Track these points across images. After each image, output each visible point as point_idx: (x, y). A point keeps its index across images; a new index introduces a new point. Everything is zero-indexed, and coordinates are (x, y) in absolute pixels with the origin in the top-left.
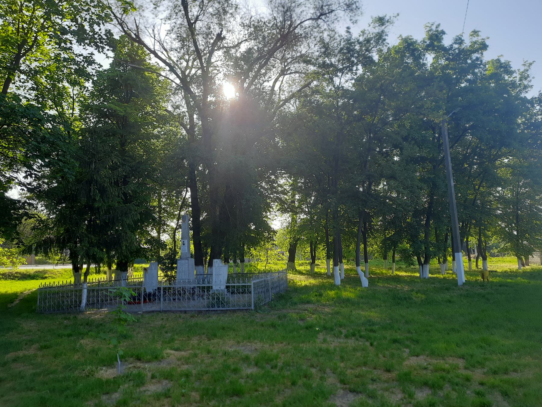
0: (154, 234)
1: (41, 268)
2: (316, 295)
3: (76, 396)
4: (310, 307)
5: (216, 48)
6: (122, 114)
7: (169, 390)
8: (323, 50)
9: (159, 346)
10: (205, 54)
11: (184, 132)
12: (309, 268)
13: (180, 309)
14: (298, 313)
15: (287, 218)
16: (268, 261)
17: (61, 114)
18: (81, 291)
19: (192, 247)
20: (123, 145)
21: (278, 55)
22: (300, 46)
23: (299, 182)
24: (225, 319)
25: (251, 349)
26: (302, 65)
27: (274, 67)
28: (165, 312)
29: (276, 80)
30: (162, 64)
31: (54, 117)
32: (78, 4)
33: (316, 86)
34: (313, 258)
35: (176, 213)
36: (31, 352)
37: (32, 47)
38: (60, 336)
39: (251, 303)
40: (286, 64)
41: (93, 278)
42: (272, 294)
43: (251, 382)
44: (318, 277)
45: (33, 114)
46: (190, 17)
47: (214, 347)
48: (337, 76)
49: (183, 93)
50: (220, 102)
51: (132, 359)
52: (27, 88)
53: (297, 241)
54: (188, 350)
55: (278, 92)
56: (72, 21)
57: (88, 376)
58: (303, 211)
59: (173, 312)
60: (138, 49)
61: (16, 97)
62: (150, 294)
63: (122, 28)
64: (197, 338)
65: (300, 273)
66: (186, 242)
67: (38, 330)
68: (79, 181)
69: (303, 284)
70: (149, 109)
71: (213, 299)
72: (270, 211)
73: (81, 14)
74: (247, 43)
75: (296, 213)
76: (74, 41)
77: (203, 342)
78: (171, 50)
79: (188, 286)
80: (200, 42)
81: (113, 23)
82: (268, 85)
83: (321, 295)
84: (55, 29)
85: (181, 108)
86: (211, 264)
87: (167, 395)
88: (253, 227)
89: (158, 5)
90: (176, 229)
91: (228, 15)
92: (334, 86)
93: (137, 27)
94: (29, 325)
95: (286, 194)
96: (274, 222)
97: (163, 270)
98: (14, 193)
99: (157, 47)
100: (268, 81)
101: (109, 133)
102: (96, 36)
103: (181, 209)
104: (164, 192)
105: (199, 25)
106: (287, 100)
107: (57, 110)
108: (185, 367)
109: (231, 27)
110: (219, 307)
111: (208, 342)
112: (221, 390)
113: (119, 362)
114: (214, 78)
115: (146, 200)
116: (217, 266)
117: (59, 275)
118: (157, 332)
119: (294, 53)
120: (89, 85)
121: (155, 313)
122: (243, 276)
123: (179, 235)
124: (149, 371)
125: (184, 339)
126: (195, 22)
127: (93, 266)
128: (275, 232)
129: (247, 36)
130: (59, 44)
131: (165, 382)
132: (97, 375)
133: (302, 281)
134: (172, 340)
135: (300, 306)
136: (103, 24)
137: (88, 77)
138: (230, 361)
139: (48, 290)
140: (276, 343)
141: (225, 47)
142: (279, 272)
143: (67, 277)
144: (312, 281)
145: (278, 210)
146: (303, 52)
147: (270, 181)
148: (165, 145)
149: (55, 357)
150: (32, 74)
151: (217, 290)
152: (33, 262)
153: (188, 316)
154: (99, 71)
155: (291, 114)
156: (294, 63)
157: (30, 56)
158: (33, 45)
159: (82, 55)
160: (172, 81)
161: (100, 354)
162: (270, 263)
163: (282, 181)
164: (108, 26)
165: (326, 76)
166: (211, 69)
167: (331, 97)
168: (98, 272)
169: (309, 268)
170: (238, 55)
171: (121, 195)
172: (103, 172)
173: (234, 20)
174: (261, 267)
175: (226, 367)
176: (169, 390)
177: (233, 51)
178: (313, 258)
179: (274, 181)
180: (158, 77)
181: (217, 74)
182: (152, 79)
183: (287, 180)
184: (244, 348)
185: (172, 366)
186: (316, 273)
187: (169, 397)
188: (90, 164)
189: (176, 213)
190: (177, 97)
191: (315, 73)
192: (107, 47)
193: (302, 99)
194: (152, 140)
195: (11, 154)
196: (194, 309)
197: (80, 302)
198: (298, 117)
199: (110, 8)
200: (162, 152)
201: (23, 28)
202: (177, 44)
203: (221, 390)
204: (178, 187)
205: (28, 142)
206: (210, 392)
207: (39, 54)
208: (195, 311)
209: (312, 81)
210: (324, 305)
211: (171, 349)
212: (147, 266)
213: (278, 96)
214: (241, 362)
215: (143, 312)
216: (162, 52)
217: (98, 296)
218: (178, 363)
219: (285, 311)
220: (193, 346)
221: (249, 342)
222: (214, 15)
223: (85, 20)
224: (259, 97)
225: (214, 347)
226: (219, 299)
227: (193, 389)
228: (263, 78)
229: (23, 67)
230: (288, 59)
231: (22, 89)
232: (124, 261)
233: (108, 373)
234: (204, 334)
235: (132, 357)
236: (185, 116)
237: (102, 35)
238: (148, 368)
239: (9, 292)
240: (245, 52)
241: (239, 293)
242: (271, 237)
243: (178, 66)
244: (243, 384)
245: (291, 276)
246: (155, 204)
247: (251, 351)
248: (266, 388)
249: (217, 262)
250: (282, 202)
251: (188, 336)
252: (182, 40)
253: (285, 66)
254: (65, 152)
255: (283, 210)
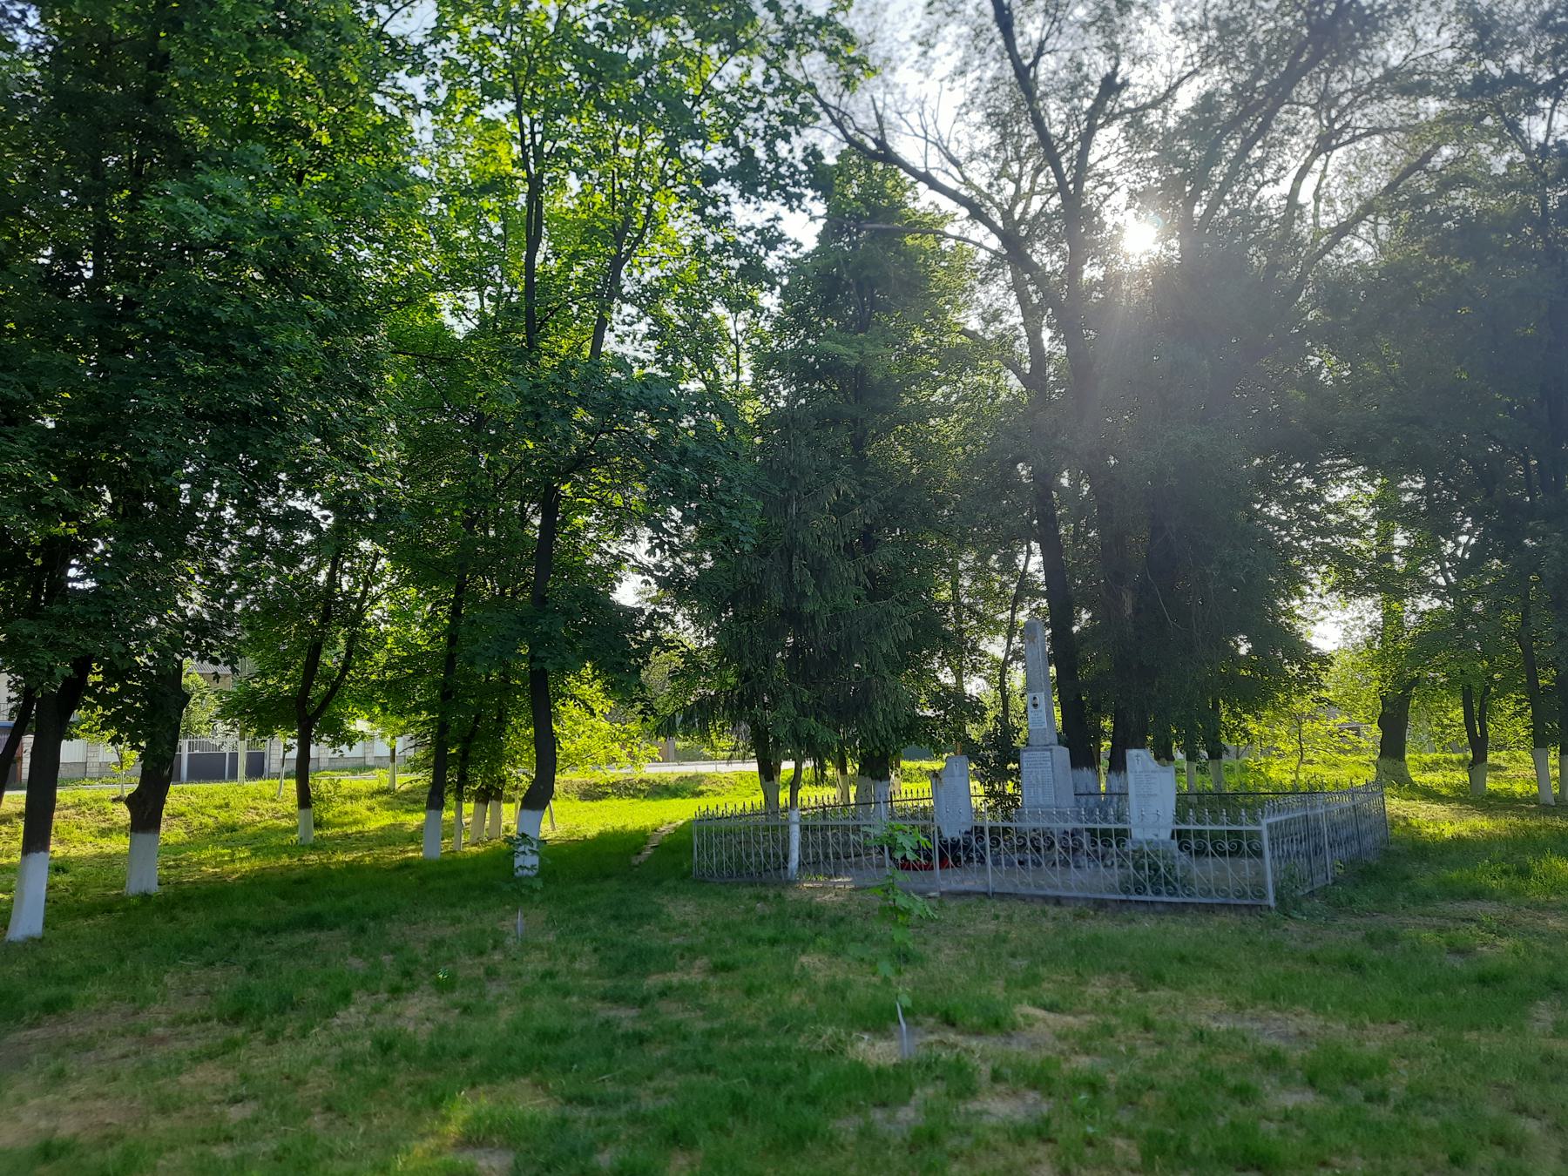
0: (947, 678)
1: (689, 769)
2: (1505, 872)
3: (811, 1100)
4: (1485, 910)
5: (1100, 122)
6: (853, 363)
7: (1047, 1121)
8: (1471, 36)
9: (997, 991)
10: (1070, 146)
11: (1014, 383)
12: (1461, 777)
13: (1041, 893)
14: (1440, 930)
15: (1366, 611)
16: (1310, 755)
17: (713, 388)
18: (786, 827)
19: (1058, 715)
20: (858, 444)
21: (1306, 90)
22: (1382, 42)
23: (1406, 491)
24: (1181, 933)
25: (1290, 1028)
26: (1394, 103)
27: (1293, 132)
28: (1002, 896)
29: (1304, 171)
30: (947, 205)
31: (698, 396)
32: (735, 99)
33: (1456, 160)
34: (1479, 746)
35: (1001, 616)
36: (694, 975)
37: (642, 233)
38: (753, 941)
39: (1264, 885)
40: (1334, 113)
41: (810, 795)
42: (1332, 862)
43: (1300, 1133)
44: (1505, 809)
45: (655, 398)
46: (1020, 51)
47: (1160, 1013)
48: (1534, 111)
49: (1009, 275)
50: (1119, 277)
51: (931, 1021)
52: (639, 336)
53: (1407, 688)
54: (1083, 1013)
55: (1311, 207)
56: (725, 145)
57: (830, 1053)
58: (1426, 586)
59: (1022, 898)
60: (883, 177)
61: (621, 363)
62: (955, 845)
63: (843, 131)
64: (1105, 979)
65: (1429, 794)
66: (1041, 698)
67: (704, 924)
68: (762, 551)
69: (1449, 831)
70: (918, 337)
71: (1138, 867)
72: (1302, 595)
73: (745, 122)
74: (1198, 80)
75: (1400, 595)
76: (734, 193)
77: (1124, 992)
78: (972, 157)
79: (1058, 826)
80: (1053, 115)
81: (819, 124)
82: (1273, 195)
83: (1524, 872)
84: (689, 176)
85: (1005, 317)
86: (1118, 764)
87: (1042, 1133)
88: (1243, 651)
89: (932, 41)
90: (1006, 663)
91: (1135, 13)
92: (1525, 149)
93: (879, 118)
94: (682, 909)
95: (1357, 534)
96: (1319, 628)
97: (981, 778)
98: (629, 592)
99: (935, 160)
100: (1276, 182)
101: (828, 419)
102: (783, 170)
103: (1015, 603)
104: (969, 557)
105: (1048, 64)
106: (1344, 229)
107: (703, 380)
108: (1083, 1062)
109: (1145, 45)
110: (1158, 893)
111: (1140, 996)
112: (1204, 1145)
113: (903, 1025)
114: (1097, 213)
115: (925, 586)
116: (1139, 768)
117: (728, 787)
118: (986, 951)
119: (1360, 73)
120: (770, 301)
121: (973, 899)
122: (1221, 801)
123: (1017, 678)
124: (984, 1059)
125: (1067, 979)
126: (1035, 63)
127: (808, 764)
128: (1325, 660)
129: (1196, 59)
130: (699, 211)
131: (1032, 1096)
132: (851, 1053)
133: (1442, 823)
134: (1031, 980)
135: (1447, 907)
136: (798, 133)
137: (770, 278)
138: (1222, 1061)
139: (704, 825)
140: (1372, 1021)
141: (1129, 111)
142: (1353, 791)
143: (748, 792)
144: (1482, 824)
145: (1332, 589)
146: (1395, 62)
147: (1296, 498)
148: (965, 429)
149: (749, 992)
150: (649, 298)
151: (1149, 843)
152: (672, 754)
153: (1066, 912)
154: (793, 262)
155: (1361, 267)
156: (1363, 105)
157: (641, 256)
158: (645, 227)
159: (752, 228)
160: (980, 245)
161: (851, 995)
162: (1311, 762)
163: (1339, 493)
164: (811, 136)
165: (1488, 121)
166: (1088, 184)
167: (1513, 186)
168: (820, 780)
169: (1461, 777)
170: (1171, 123)
171: (863, 578)
172: (817, 524)
173: (1154, 22)
174: (1280, 772)
175: (1213, 1079)
176: (1047, 1121)
177: (1154, 115)
178: (1479, 746)
179: (1314, 497)
180: (938, 241)
181: (1106, 197)
182: (925, 252)
183: (1359, 487)
184: (1258, 1025)
185: (1045, 1053)
186: (1493, 795)
187: (1050, 1140)
188: (786, 504)
189: (1001, 616)
190: (993, 289)
191: (1444, 119)
192: (810, 193)
193: (1405, 215)
194: (932, 422)
195: (618, 501)
196: (1081, 895)
197: (786, 857)
198: (1392, 280)
199: (811, 87)
200: (959, 449)
201: (622, 191)
202: (987, 138)
203: (1204, 1145)
204: (1009, 541)
205: (651, 467)
206: (1172, 1146)
207: (657, 246)
208: (1086, 899)
209: (1437, 147)
210: (1540, 908)
211: (1035, 1004)
212: (937, 765)
213: (1310, 221)
214: (1258, 1068)
215: (942, 893)
216: (946, 172)
217: (825, 843)
218: (1060, 1046)
219: (1391, 920)
220: (1096, 1002)
221: (1275, 1008)
222: (1093, 23)
223: (755, 135)
224: (1245, 236)
225: (1160, 1013)
226: (1157, 870)
227: (1117, 1129)
228: (1258, 176)
229: (628, 288)
230: (1342, 94)
231: (628, 340)
232: (877, 753)
233: (877, 1050)
234: (1123, 969)
235: (931, 1014)
236: (1018, 337)
237: (795, 162)
238: (981, 1051)
239: (630, 827)
240: (1193, 110)
241: (1222, 854)
242: (1310, 678)
243: (992, 200)
244: (1274, 1136)
245: (1395, 805)
246: (944, 595)
247: (1287, 1037)
248: (1358, 1160)
249: (1140, 759)
250: (1344, 561)
251: (1077, 972)
252: (999, 121)
253: (1332, 122)
254: (731, 480)
255: (1350, 588)
